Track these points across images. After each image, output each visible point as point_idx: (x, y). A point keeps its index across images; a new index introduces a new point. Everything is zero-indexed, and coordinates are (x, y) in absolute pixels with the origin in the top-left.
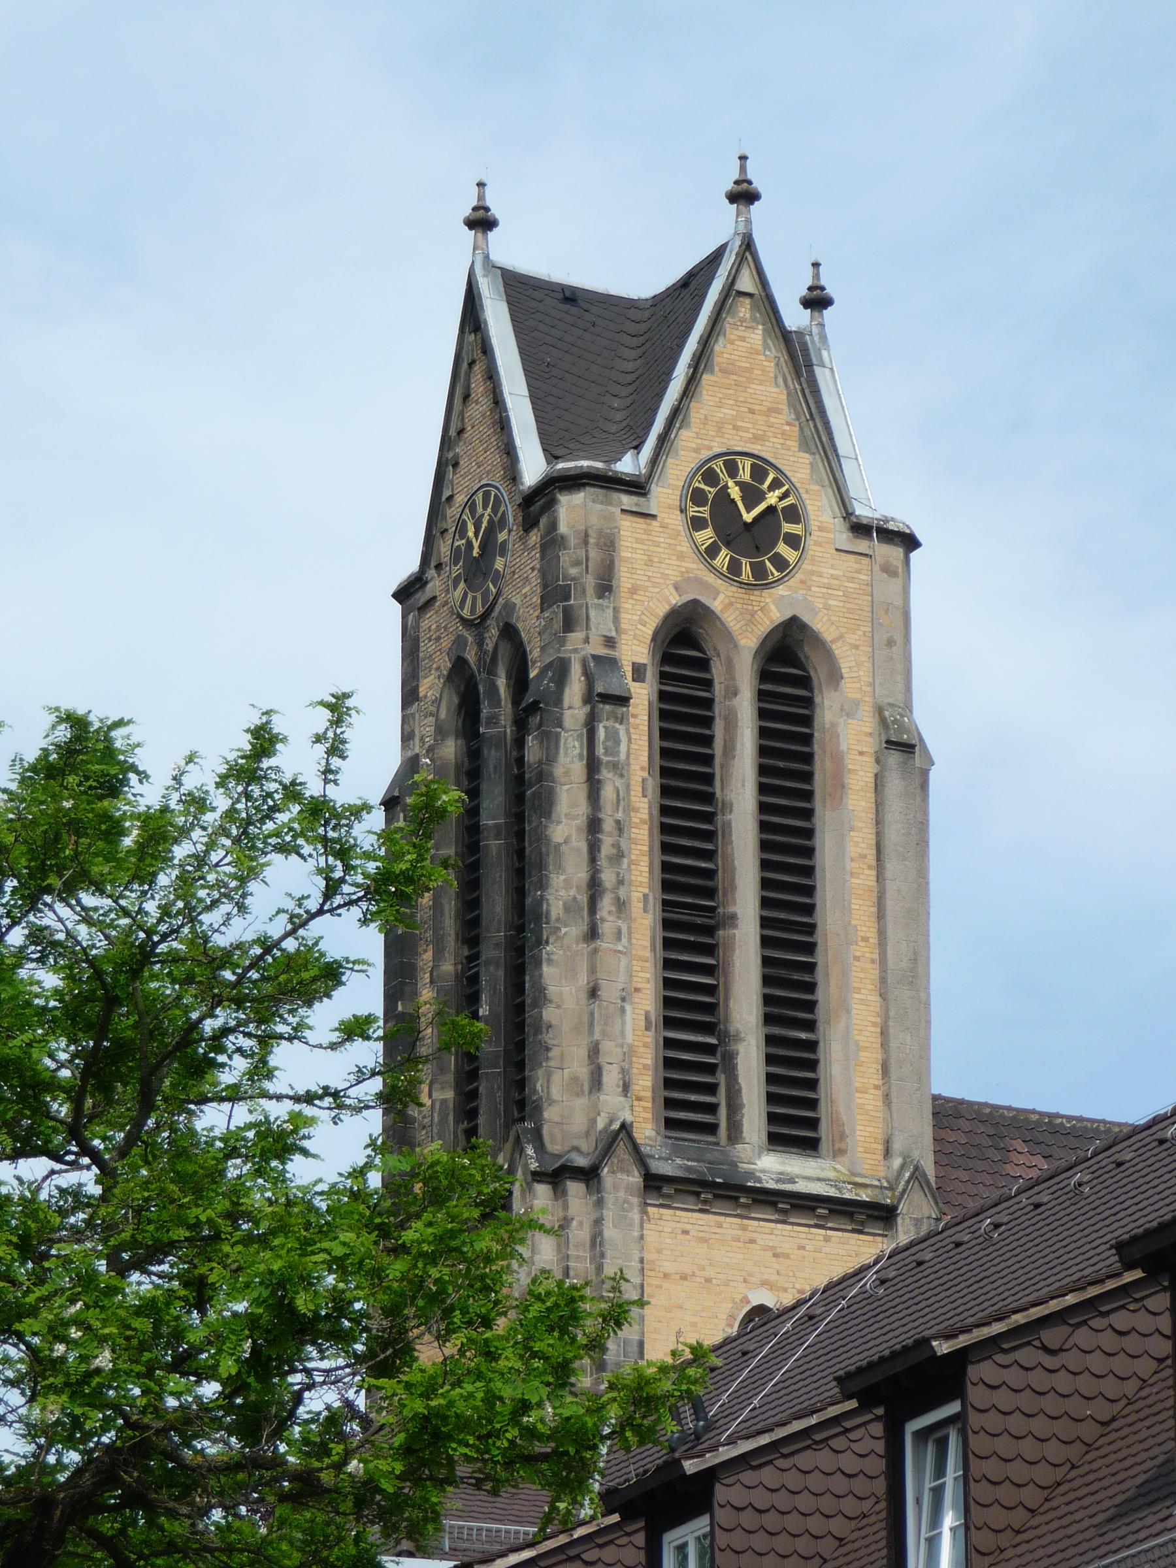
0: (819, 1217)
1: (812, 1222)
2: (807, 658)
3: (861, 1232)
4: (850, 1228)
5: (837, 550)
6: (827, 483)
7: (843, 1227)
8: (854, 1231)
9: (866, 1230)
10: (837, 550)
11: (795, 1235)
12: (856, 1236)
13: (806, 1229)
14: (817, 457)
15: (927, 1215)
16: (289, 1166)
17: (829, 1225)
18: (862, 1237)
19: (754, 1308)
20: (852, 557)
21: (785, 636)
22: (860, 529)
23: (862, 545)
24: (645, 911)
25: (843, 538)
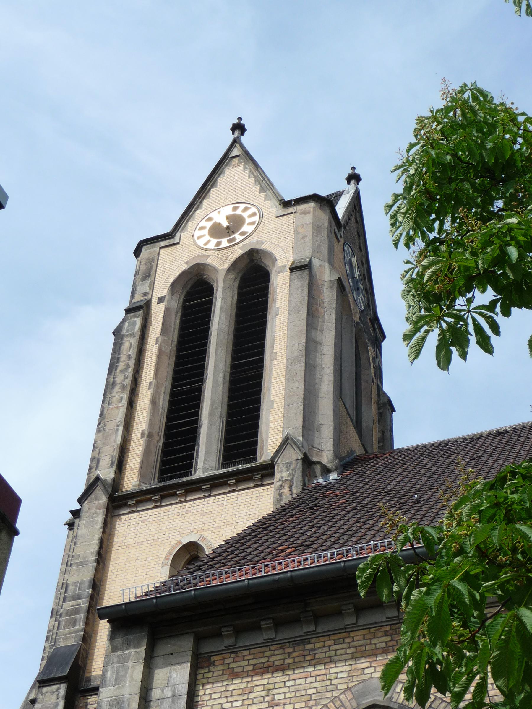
0: (230, 485)
1: (227, 490)
2: (265, 264)
3: (261, 485)
4: (253, 485)
5: (277, 217)
6: (272, 197)
7: (248, 486)
8: (256, 486)
9: (265, 483)
10: (277, 217)
11: (217, 500)
12: (259, 489)
13: (225, 496)
14: (268, 191)
15: (295, 458)
16: (101, 622)
17: (239, 488)
18: (262, 488)
19: (184, 545)
20: (285, 217)
21: (252, 261)
22: (286, 204)
23: (291, 210)
24: (149, 389)
25: (282, 211)
